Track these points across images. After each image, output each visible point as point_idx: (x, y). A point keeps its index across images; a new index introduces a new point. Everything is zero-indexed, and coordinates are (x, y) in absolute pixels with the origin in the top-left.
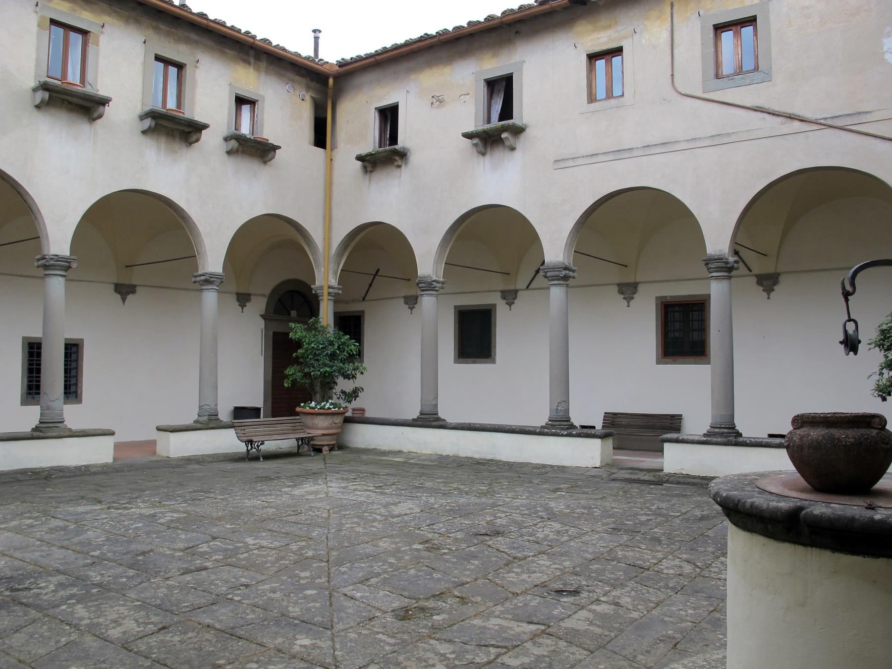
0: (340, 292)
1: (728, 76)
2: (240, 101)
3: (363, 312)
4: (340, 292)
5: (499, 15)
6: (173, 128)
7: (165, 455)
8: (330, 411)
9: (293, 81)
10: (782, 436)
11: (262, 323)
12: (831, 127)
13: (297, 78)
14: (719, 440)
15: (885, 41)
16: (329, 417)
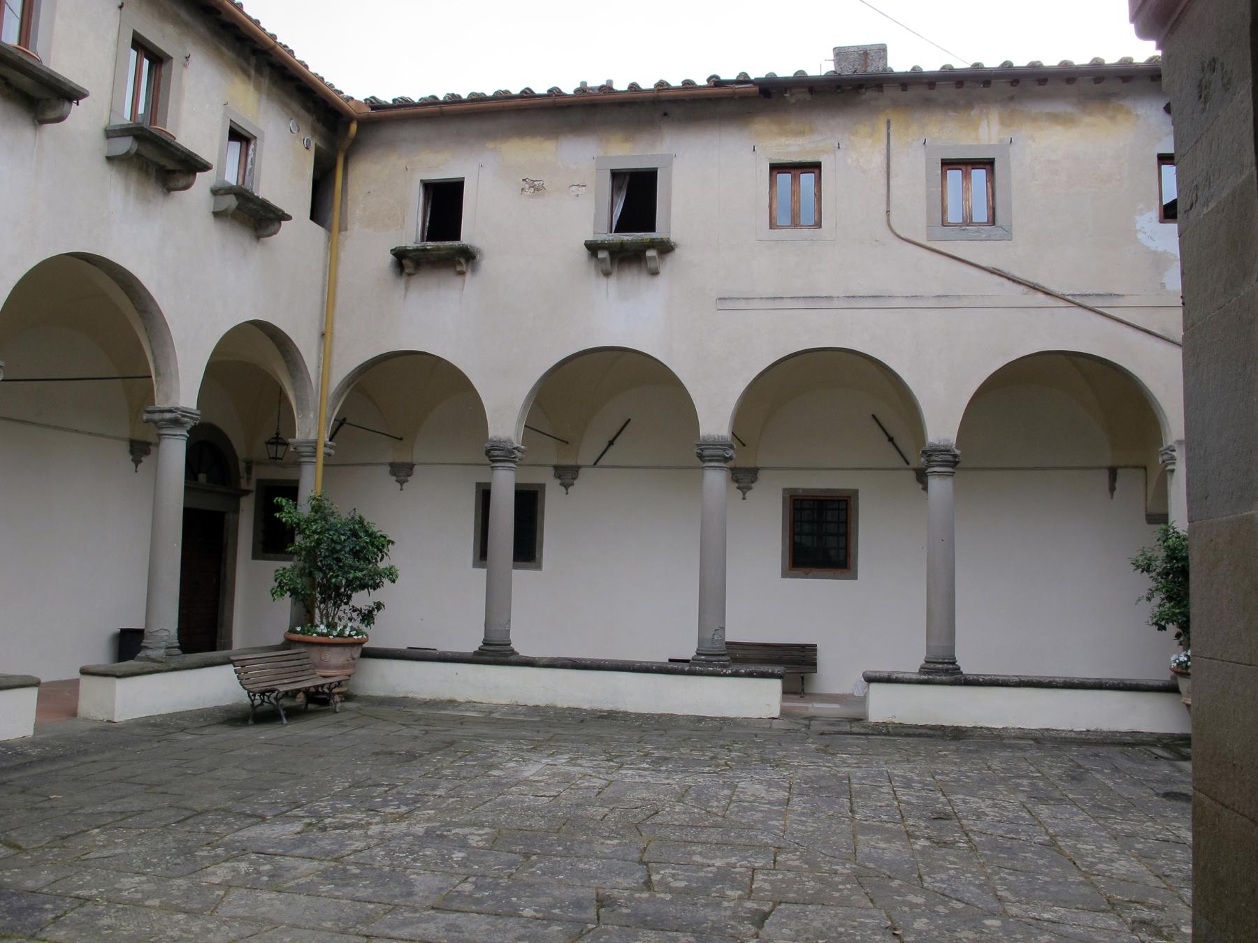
0: (332, 452)
1: (955, 225)
2: (236, 134)
4: (332, 452)
6: (156, 160)
7: (101, 716)
8: (350, 640)
9: (297, 116)
10: (687, 661)
12: (1080, 306)
13: (303, 113)
14: (944, 678)
15: (1137, 218)
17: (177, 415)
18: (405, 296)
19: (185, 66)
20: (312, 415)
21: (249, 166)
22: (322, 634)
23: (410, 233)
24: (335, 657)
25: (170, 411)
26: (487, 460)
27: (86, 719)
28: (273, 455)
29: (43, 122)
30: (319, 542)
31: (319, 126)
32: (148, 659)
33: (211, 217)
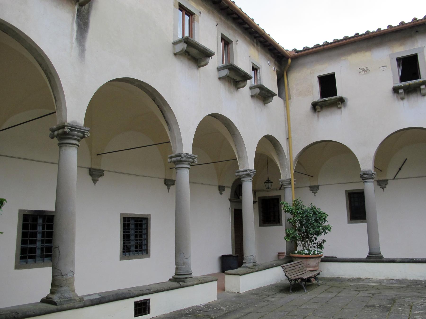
3: (280, 196)
5: (387, 28)
6: (235, 77)
7: (235, 290)
8: (318, 255)
11: (229, 203)
13: (271, 58)
16: (317, 259)
17: (249, 172)
18: (318, 120)
19: (237, 44)
20: (287, 169)
21: (258, 79)
22: (306, 254)
23: (316, 96)
24: (312, 263)
25: (246, 171)
26: (361, 179)
27: (229, 292)
28: (267, 187)
29: (200, 67)
30: (302, 217)
31: (276, 62)
32: (247, 267)
33: (250, 97)
